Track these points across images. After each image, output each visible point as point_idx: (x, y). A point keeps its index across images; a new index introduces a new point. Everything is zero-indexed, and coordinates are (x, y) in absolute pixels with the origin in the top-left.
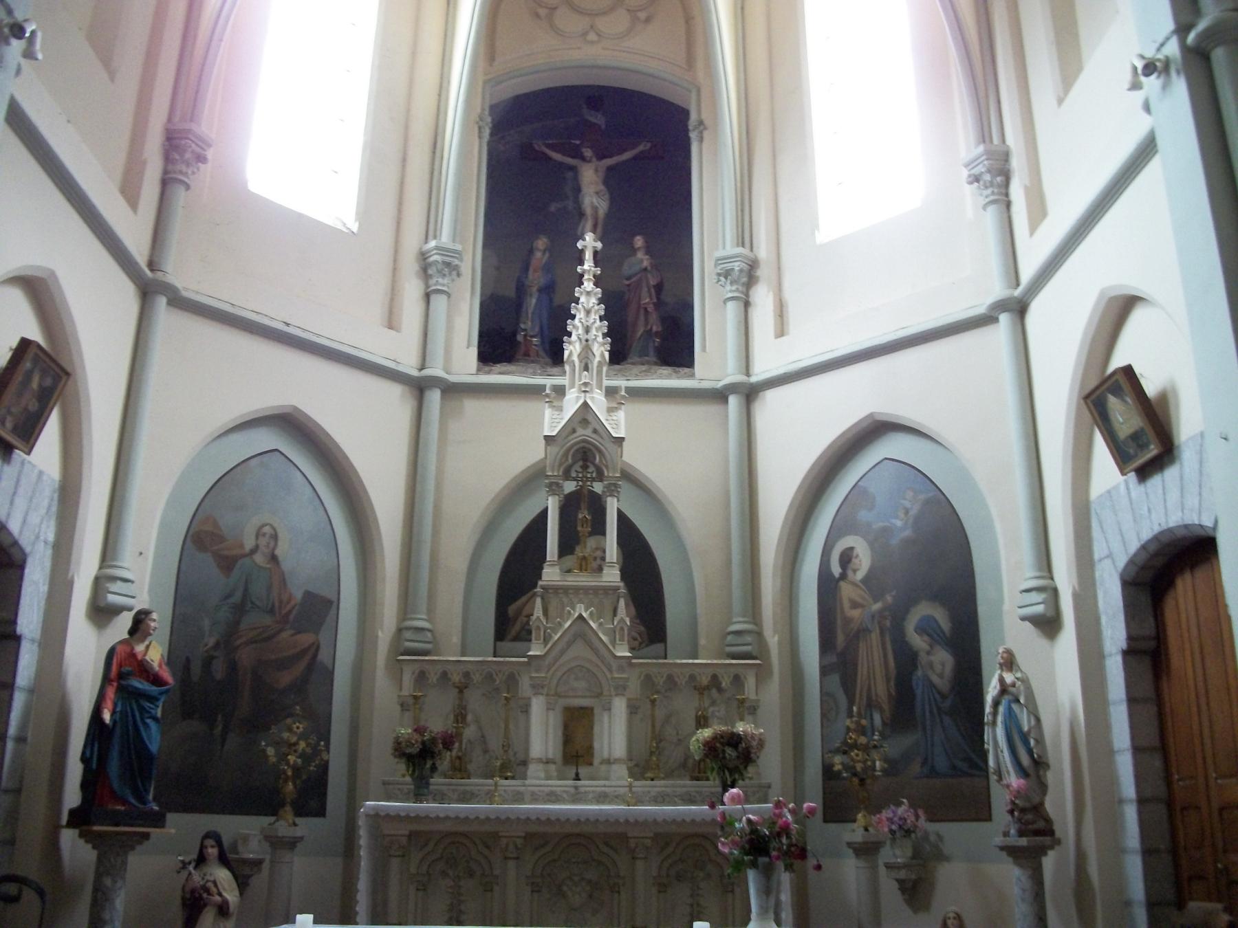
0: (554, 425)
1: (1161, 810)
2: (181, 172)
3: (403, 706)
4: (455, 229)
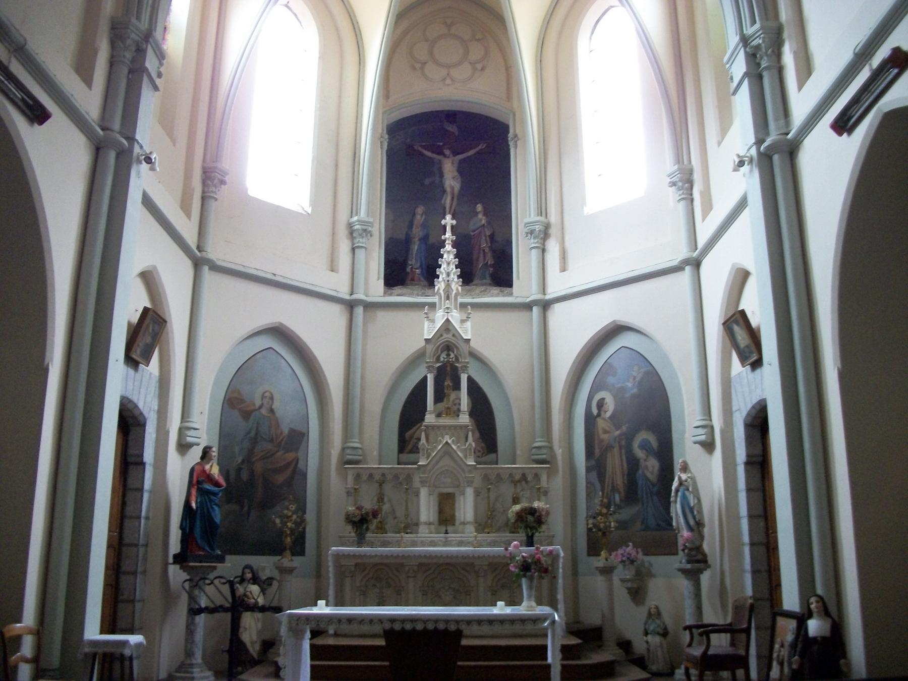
0: (430, 331)
1: (763, 549)
2: (212, 192)
3: (348, 494)
4: (368, 207)
